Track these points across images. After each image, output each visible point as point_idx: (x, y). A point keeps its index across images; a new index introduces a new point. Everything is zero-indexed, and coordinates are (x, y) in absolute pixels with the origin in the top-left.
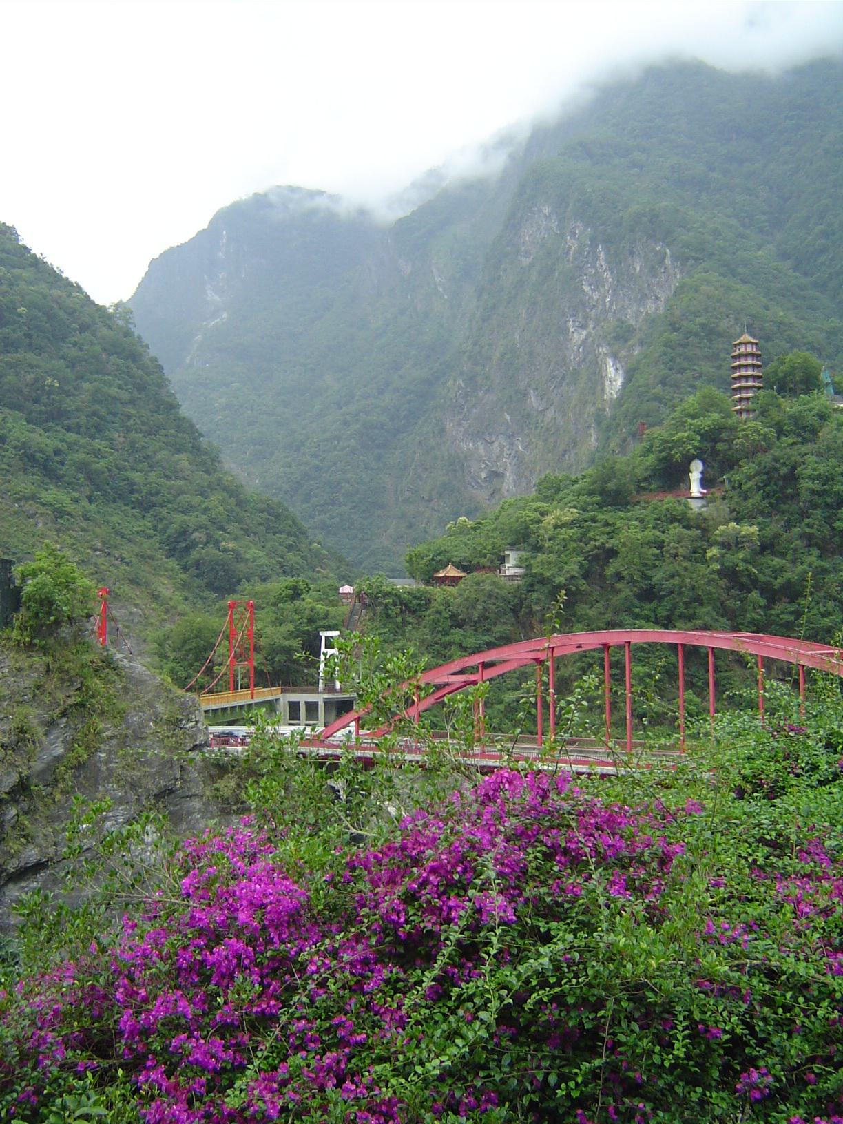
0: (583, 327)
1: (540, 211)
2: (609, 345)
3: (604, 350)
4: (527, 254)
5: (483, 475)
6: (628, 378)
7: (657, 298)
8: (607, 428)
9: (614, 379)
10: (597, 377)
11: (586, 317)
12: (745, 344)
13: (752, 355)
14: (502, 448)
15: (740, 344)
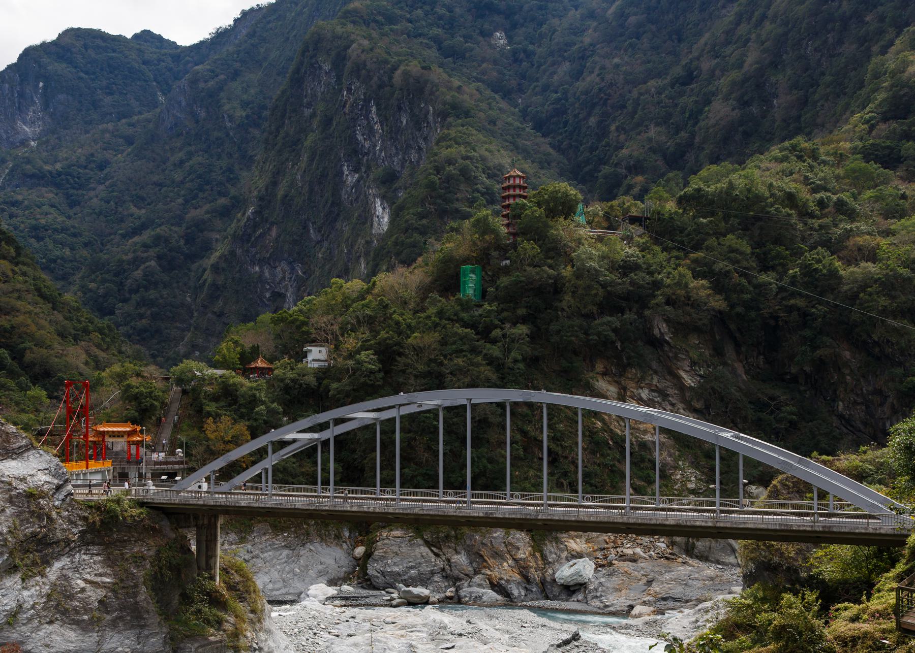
1: (320, 68)
4: (309, 105)
5: (268, 295)
7: (420, 149)
10: (367, 217)
11: (359, 163)
12: (514, 177)
14: (284, 272)
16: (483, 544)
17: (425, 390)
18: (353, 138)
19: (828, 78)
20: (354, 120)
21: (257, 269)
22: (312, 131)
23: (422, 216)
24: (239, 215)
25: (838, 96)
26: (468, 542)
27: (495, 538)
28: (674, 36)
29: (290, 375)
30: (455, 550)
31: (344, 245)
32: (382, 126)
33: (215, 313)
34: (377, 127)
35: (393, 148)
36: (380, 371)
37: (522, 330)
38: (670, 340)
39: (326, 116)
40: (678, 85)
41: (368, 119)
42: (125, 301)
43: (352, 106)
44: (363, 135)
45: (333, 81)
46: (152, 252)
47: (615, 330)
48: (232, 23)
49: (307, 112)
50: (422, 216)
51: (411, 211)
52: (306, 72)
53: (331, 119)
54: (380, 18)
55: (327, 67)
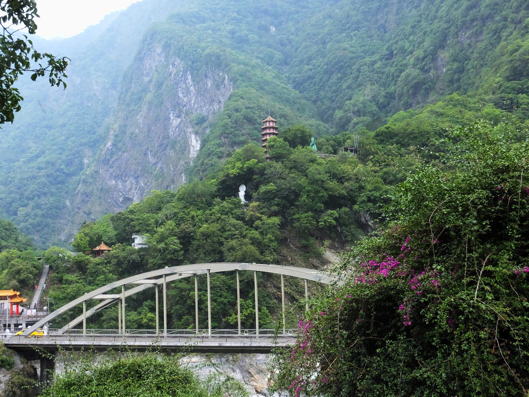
0: (179, 117)
1: (155, 51)
2: (193, 127)
3: (190, 130)
4: (148, 75)
5: (121, 199)
6: (203, 146)
7: (220, 102)
8: (190, 173)
9: (195, 144)
11: (181, 111)
12: (269, 122)
13: (273, 128)
14: (132, 184)
15: (266, 122)
16: (251, 364)
17: (212, 262)
18: (176, 95)
19: (475, 55)
20: (177, 84)
21: (114, 182)
22: (150, 92)
23: (220, 145)
24: (101, 147)
25: (482, 66)
26: (241, 364)
27: (258, 360)
28: (381, 30)
29: (123, 254)
30: (233, 369)
31: (171, 165)
32: (195, 88)
33: (85, 212)
34: (192, 88)
35: (203, 102)
36: (181, 249)
37: (276, 220)
38: (372, 225)
39: (159, 81)
40: (384, 60)
41: (185, 83)
42: (25, 206)
43: (175, 75)
44: (183, 93)
45: (163, 59)
46: (43, 172)
47: (336, 219)
48: (99, 23)
49: (146, 79)
50: (220, 145)
51: (213, 143)
52: (145, 54)
53: (162, 84)
54: (194, 19)
55: (159, 50)
